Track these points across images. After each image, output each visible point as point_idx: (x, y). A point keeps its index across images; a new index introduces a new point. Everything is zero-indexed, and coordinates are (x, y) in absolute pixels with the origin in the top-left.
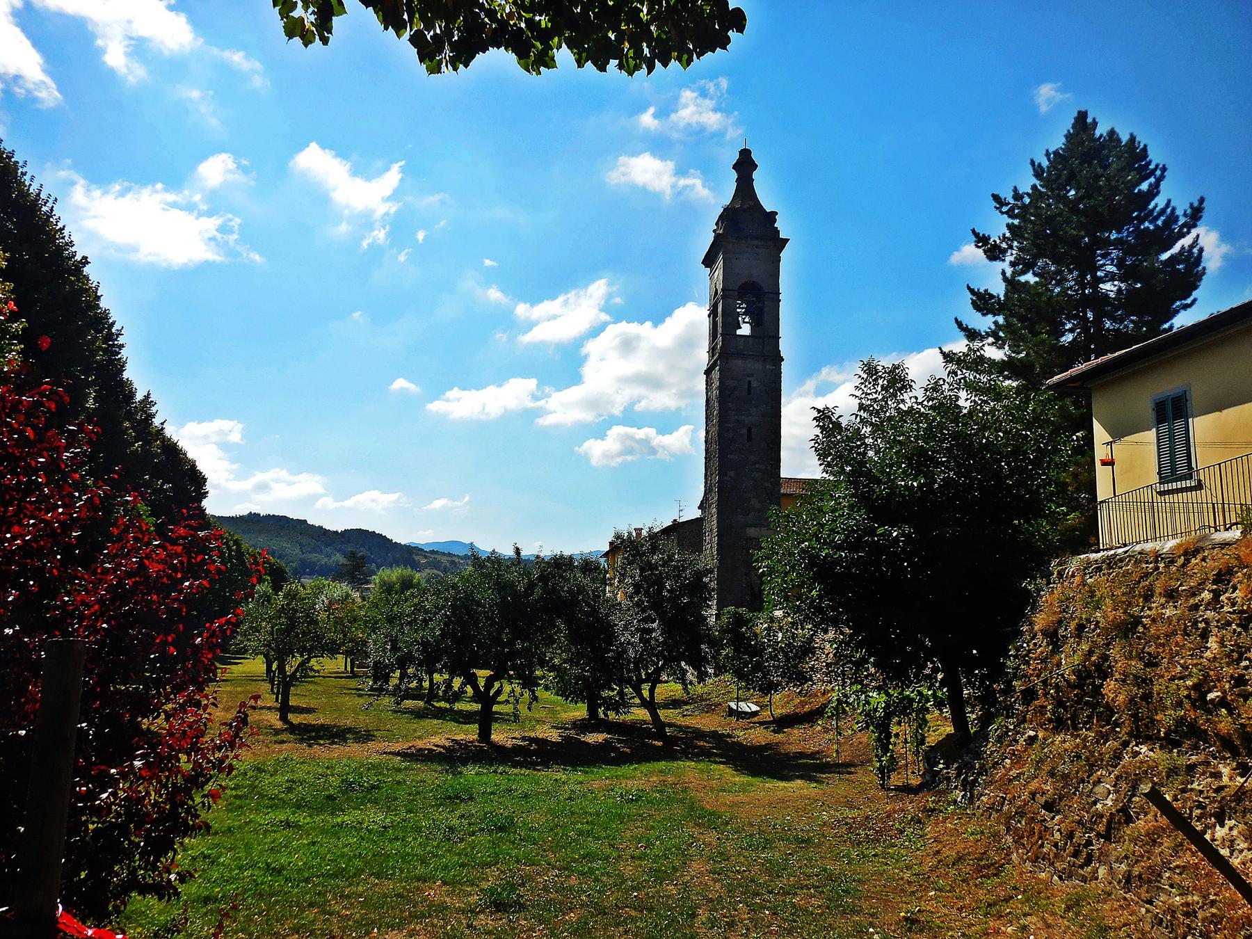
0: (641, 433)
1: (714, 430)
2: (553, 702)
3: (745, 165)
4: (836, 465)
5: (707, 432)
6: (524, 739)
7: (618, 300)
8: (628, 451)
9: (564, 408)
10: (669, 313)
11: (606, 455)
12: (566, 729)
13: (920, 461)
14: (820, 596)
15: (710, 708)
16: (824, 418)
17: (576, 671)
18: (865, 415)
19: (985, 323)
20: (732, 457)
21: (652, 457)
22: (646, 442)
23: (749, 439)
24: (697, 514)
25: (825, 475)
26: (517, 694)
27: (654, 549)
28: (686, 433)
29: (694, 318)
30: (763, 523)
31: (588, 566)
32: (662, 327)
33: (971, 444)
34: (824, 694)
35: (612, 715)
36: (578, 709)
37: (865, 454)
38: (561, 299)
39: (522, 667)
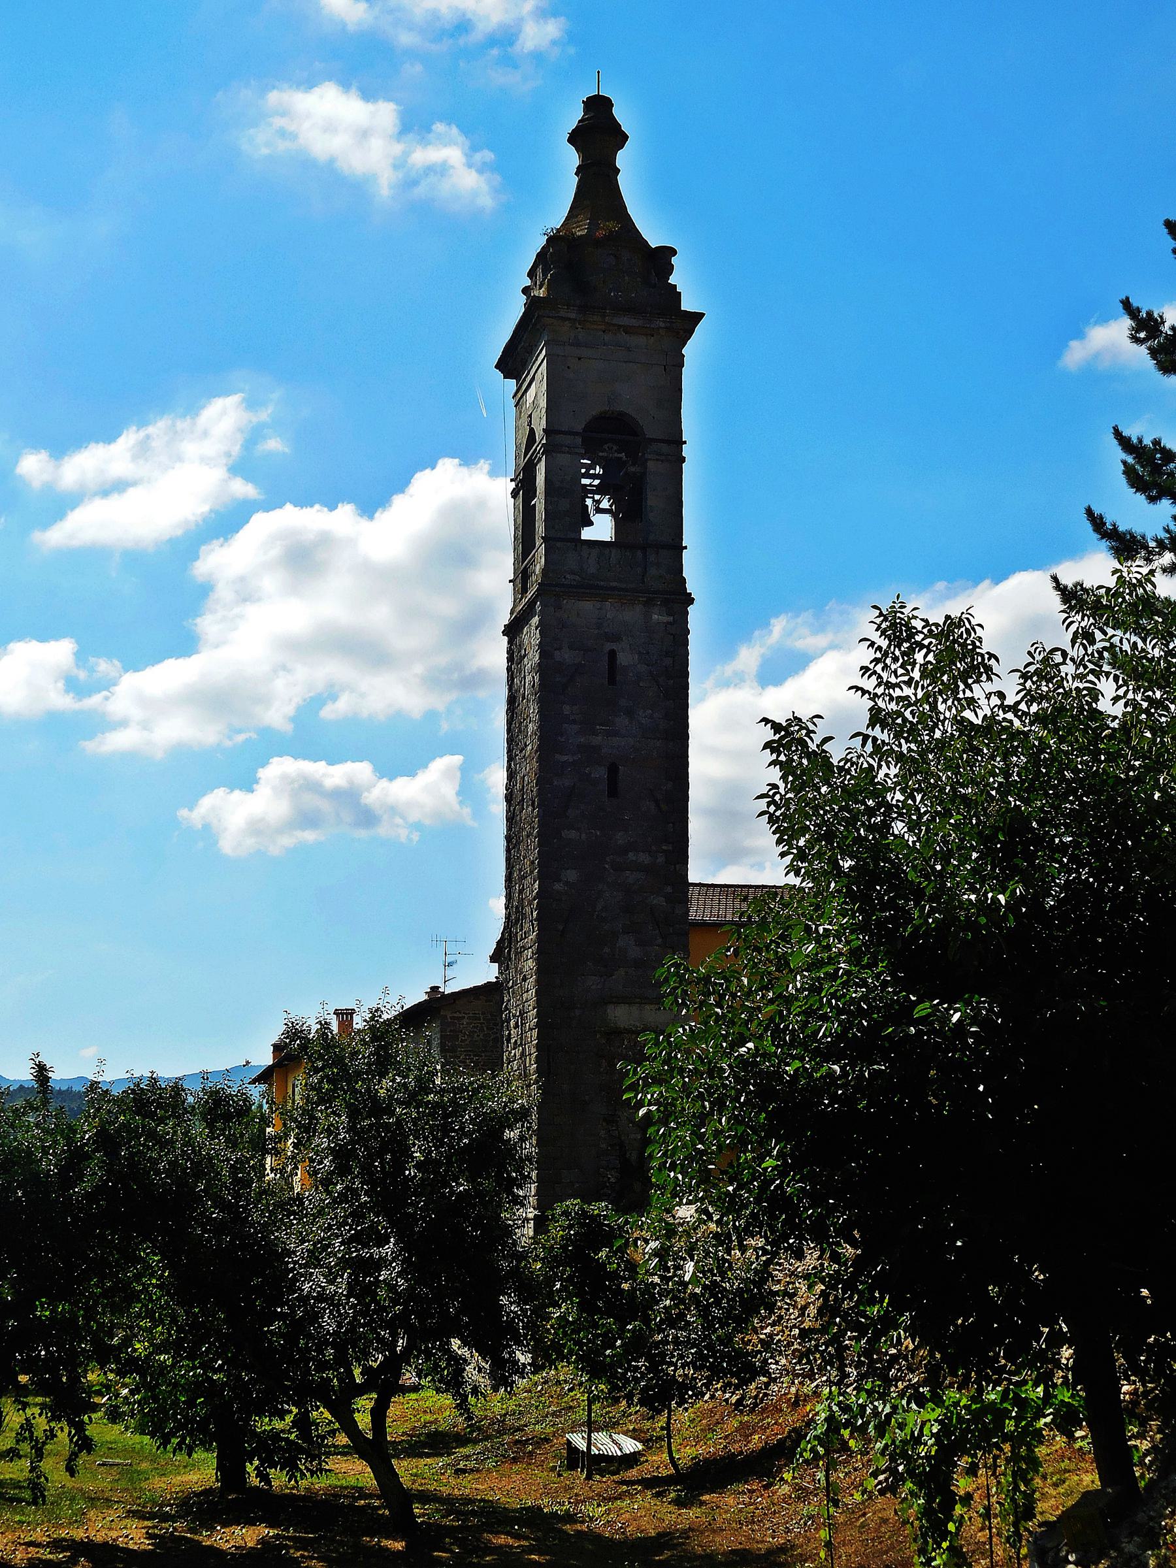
0: (335, 775)
1: (529, 769)
2: (129, 1451)
3: (598, 134)
4: (820, 855)
5: (511, 775)
6: (56, 1545)
7: (274, 444)
8: (306, 819)
9: (152, 709)
10: (401, 484)
11: (256, 828)
12: (165, 1518)
13: (1011, 845)
14: (782, 1172)
15: (522, 1449)
16: (788, 739)
17: (188, 1371)
18: (883, 736)
19: (1149, 518)
20: (573, 834)
21: (362, 834)
22: (348, 796)
23: (613, 791)
24: (489, 973)
25: (793, 880)
26: (39, 1434)
27: (383, 1063)
28: (447, 773)
29: (469, 497)
30: (647, 993)
31: (221, 1108)
32: (384, 518)
33: (1129, 802)
34: (796, 1404)
35: (279, 1479)
36: (194, 1466)
37: (886, 826)
38: (128, 439)
39: (51, 1364)
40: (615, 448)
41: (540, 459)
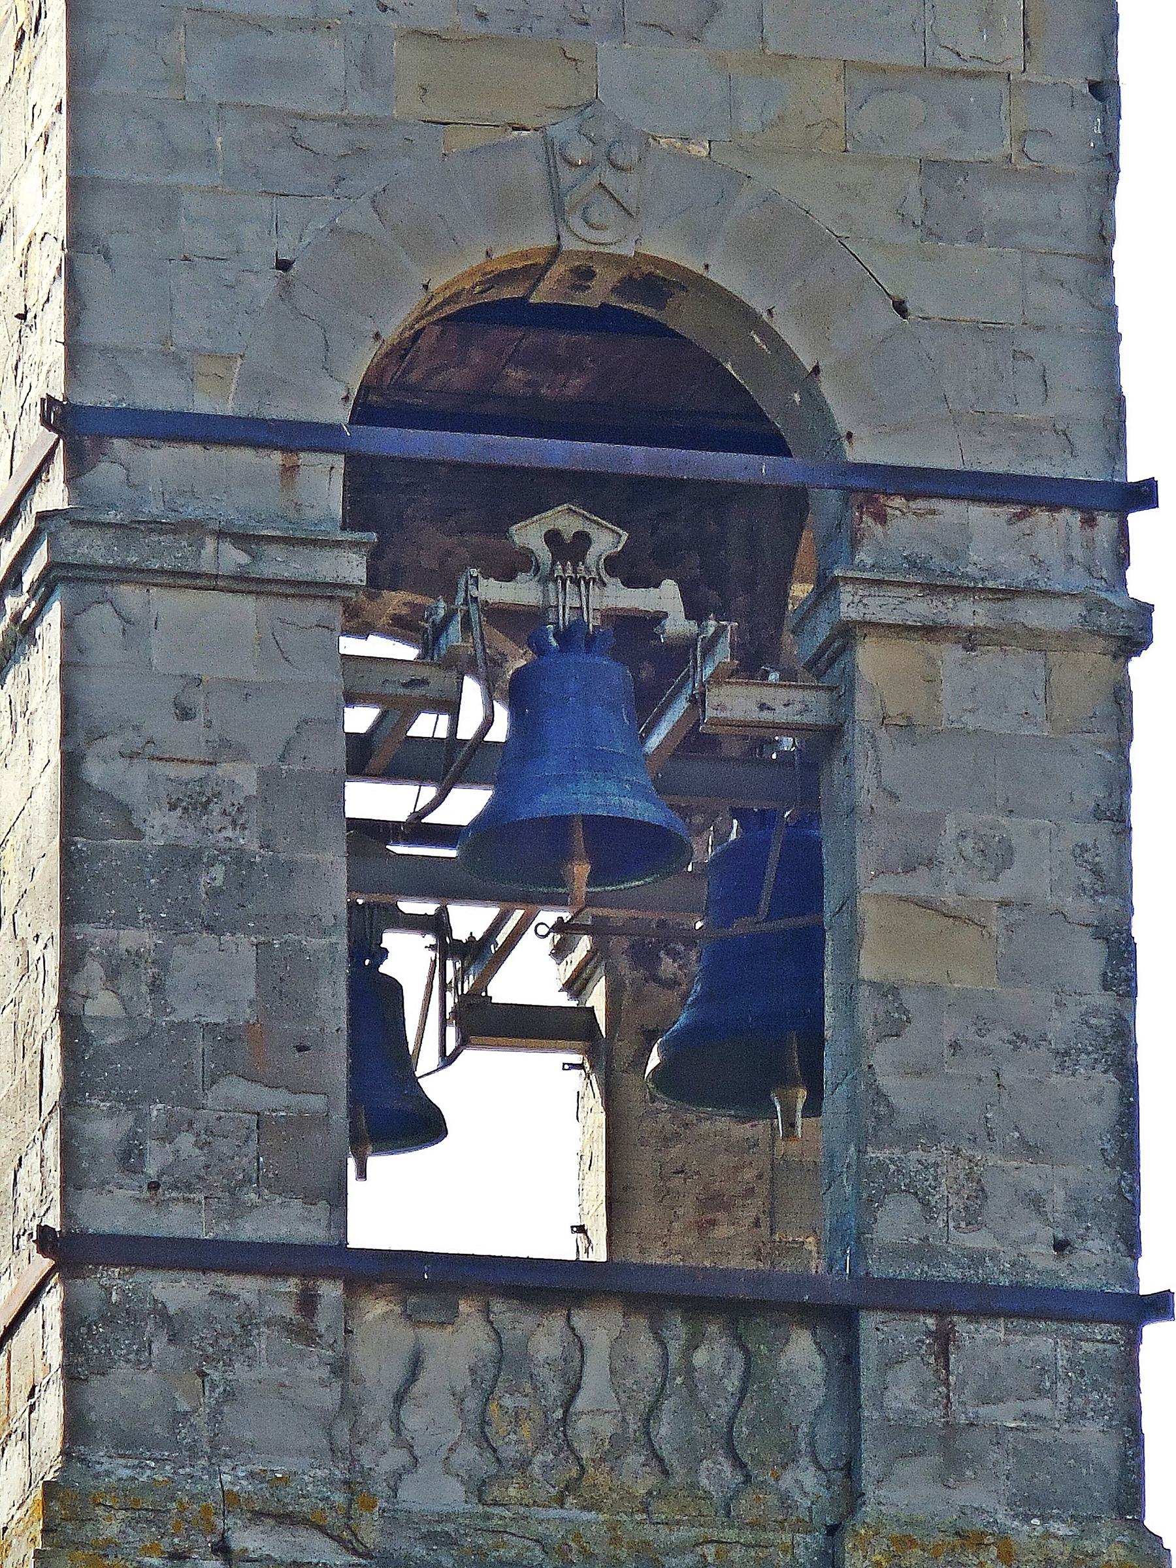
40: (606, 541)
41: (25, 630)
